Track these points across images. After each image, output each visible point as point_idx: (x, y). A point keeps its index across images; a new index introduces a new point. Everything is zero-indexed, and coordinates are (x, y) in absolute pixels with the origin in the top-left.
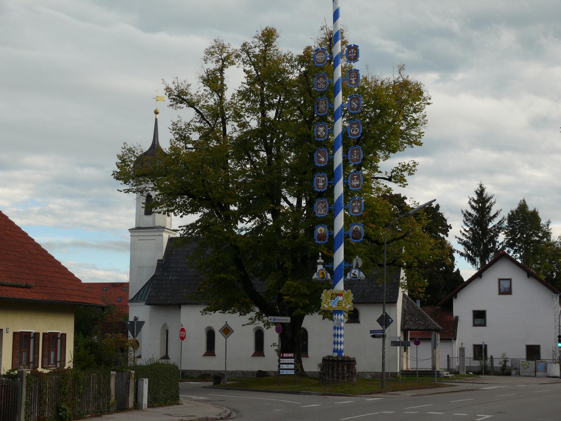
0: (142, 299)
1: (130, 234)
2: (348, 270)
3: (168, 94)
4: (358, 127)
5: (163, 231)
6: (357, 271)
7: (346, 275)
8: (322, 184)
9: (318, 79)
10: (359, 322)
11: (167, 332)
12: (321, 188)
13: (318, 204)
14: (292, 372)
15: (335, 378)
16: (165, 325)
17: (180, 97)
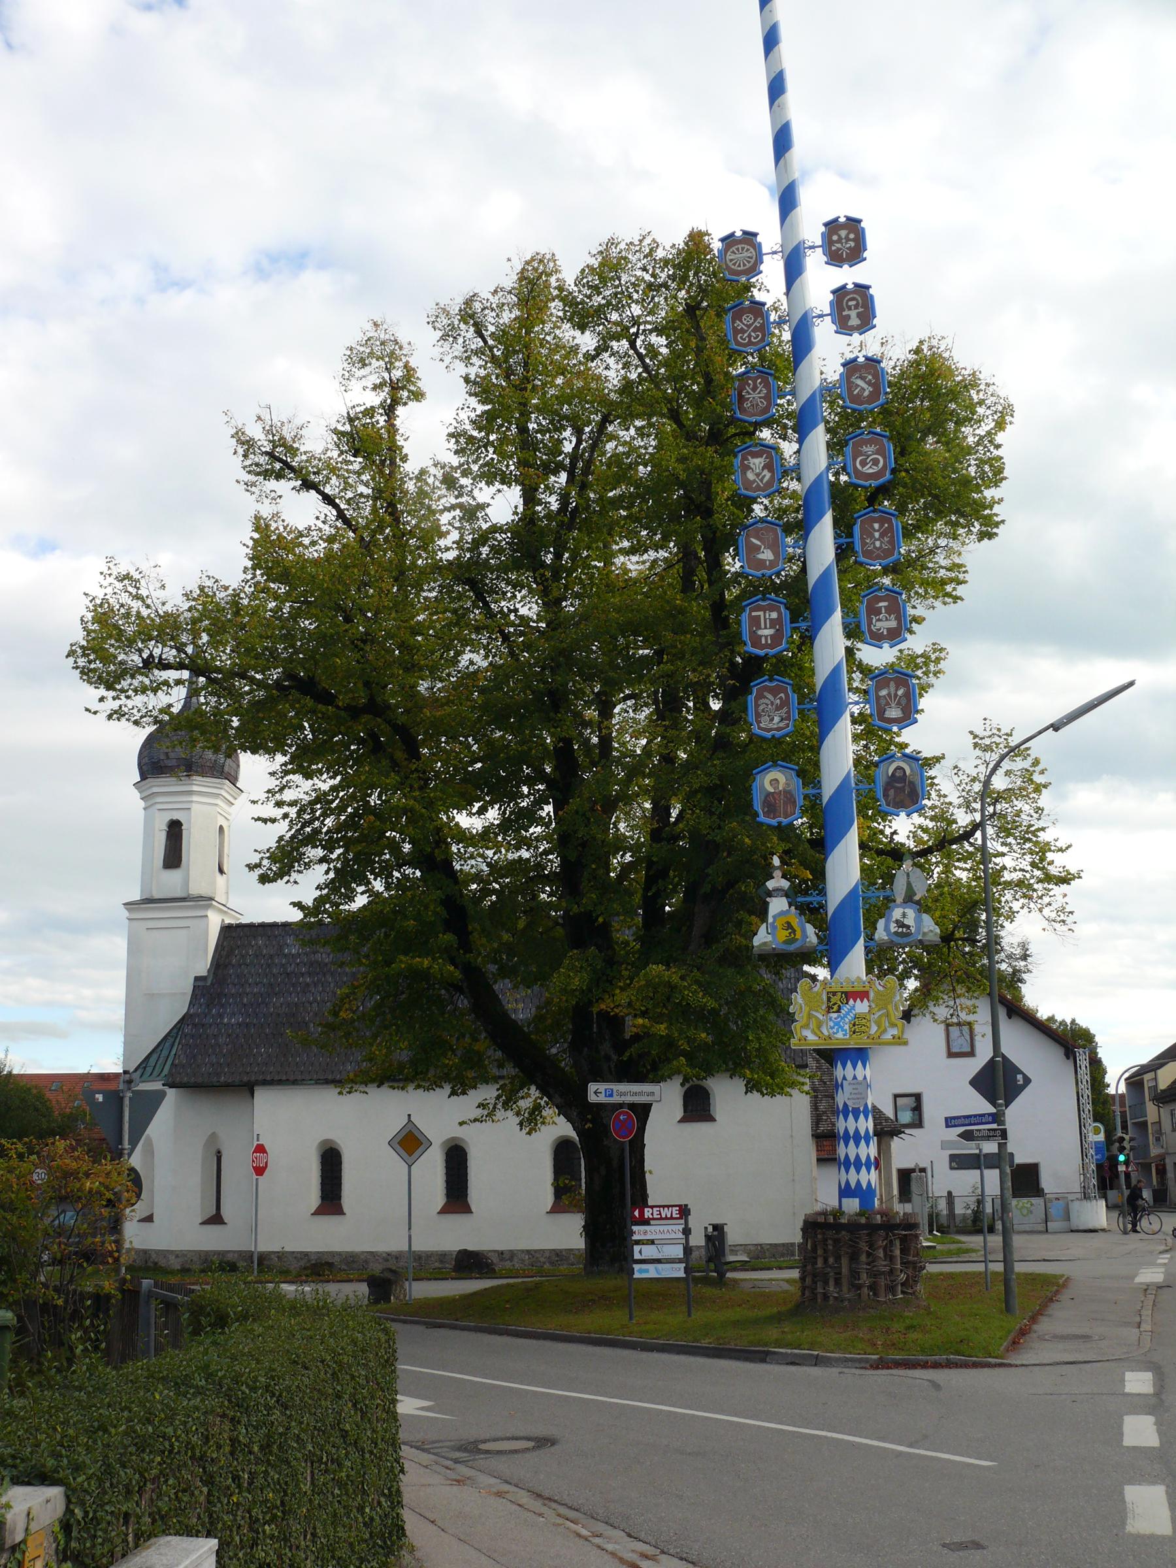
0: (155, 1073)
1: (126, 914)
2: (876, 912)
3: (241, 451)
4: (881, 451)
5: (210, 906)
6: (911, 913)
7: (871, 925)
8: (769, 632)
9: (738, 316)
10: (711, 1119)
11: (219, 1156)
12: (766, 646)
13: (760, 696)
14: (678, 1271)
15: (865, 1290)
16: (213, 1137)
17: (278, 460)
